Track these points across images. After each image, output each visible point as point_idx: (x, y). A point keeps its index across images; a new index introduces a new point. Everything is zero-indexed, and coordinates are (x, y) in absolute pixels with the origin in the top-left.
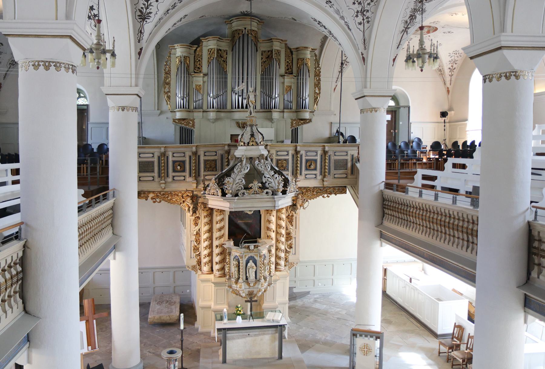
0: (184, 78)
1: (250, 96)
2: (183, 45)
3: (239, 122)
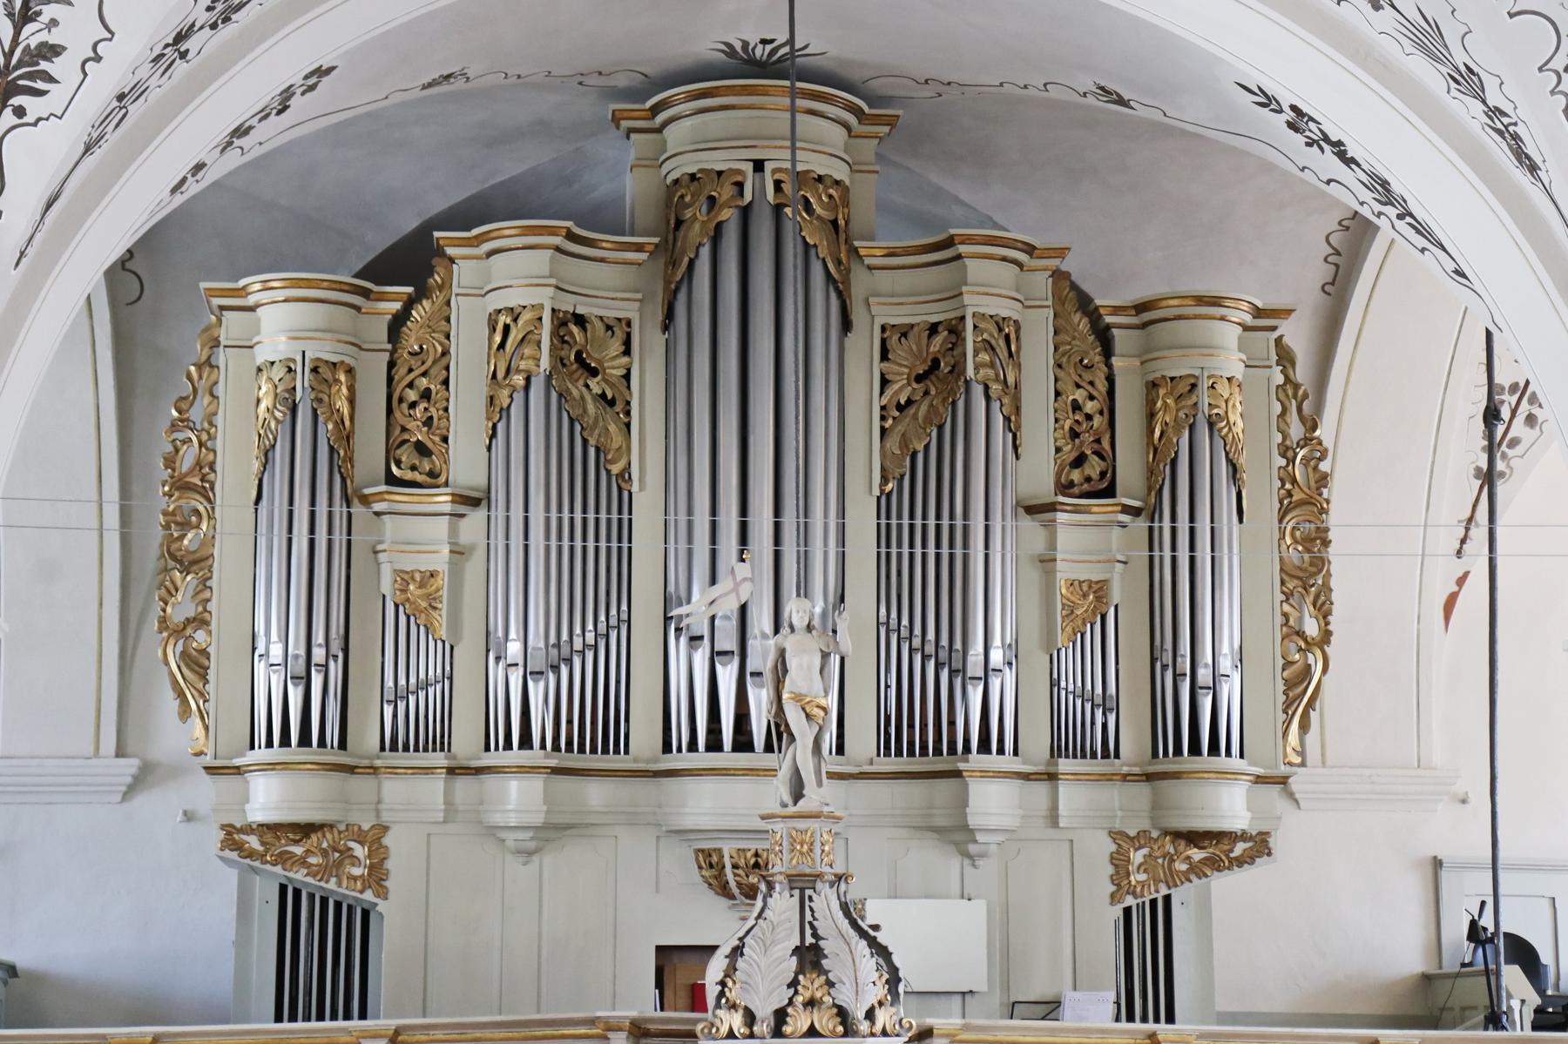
0: (312, 530)
2: (309, 283)
3: (719, 851)
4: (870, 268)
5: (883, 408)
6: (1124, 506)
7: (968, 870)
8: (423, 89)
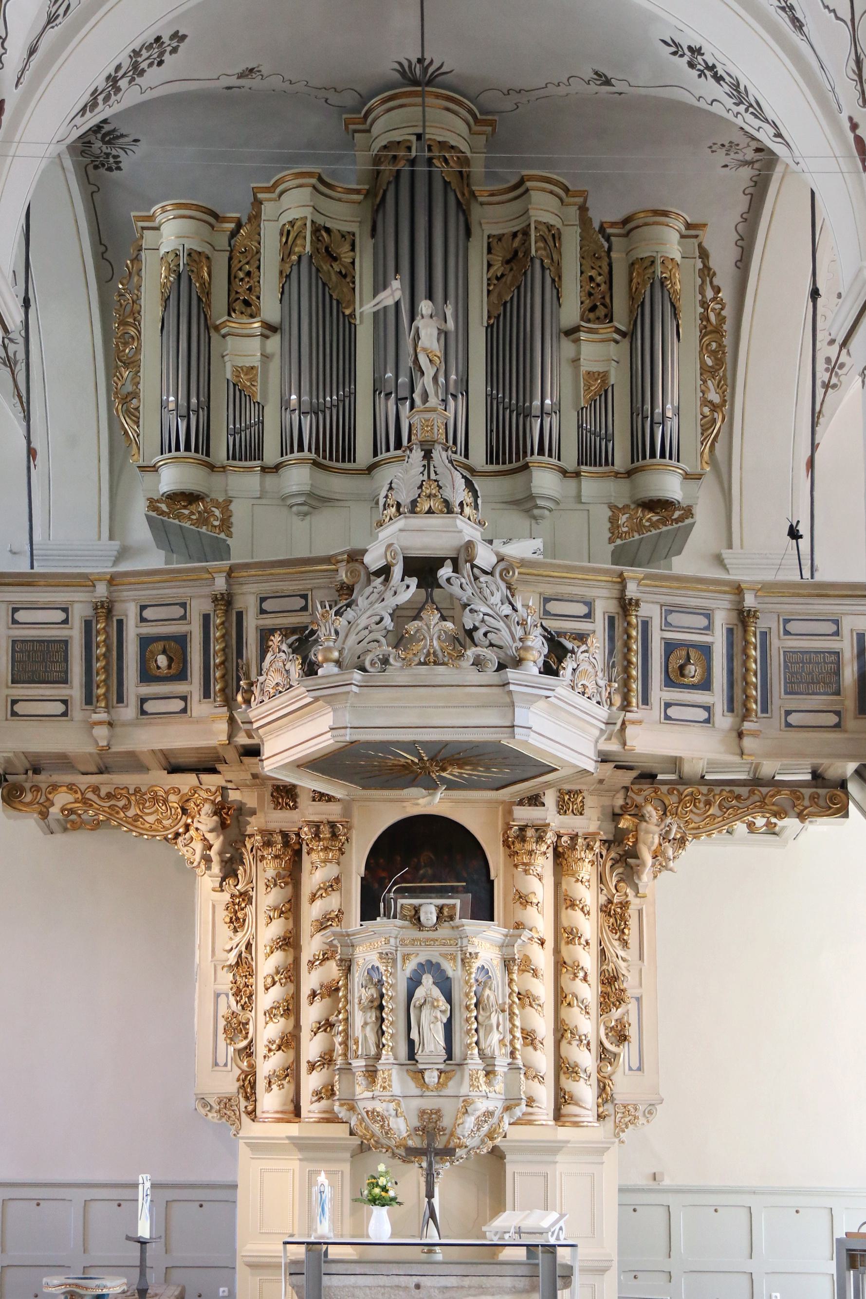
1: (423, 333)
4: (482, 204)
5: (489, 279)
6: (616, 328)
7: (534, 526)
8: (239, 78)
